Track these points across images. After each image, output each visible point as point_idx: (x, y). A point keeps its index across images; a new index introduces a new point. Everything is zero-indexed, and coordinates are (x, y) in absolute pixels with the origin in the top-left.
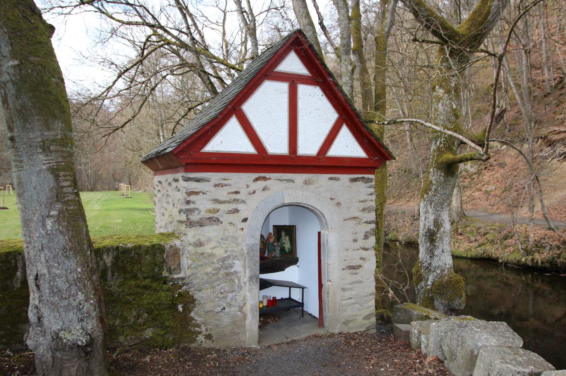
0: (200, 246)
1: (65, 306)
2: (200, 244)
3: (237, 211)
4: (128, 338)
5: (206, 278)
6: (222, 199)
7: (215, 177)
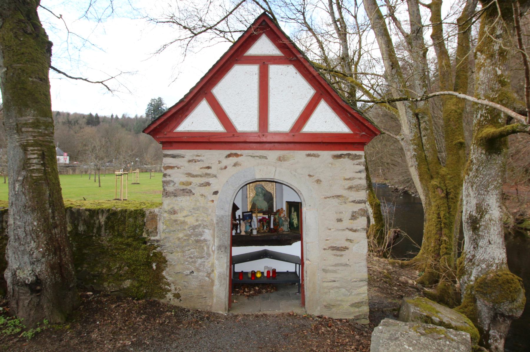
0: (174, 214)
1: (22, 250)
2: (174, 212)
3: (208, 184)
4: (110, 285)
5: (177, 242)
6: (195, 173)
7: (189, 153)
